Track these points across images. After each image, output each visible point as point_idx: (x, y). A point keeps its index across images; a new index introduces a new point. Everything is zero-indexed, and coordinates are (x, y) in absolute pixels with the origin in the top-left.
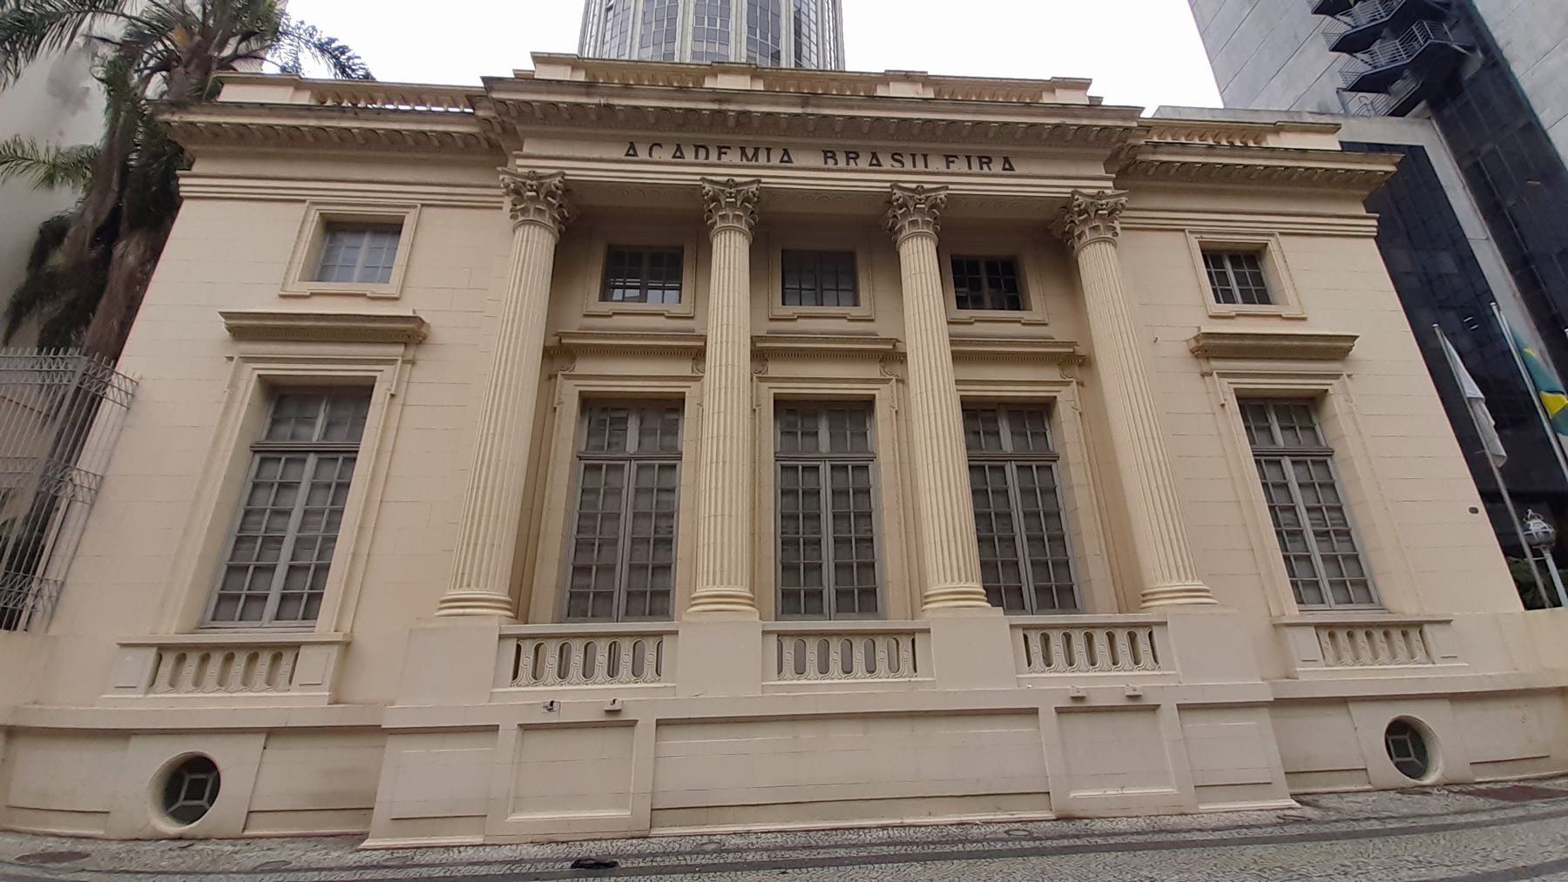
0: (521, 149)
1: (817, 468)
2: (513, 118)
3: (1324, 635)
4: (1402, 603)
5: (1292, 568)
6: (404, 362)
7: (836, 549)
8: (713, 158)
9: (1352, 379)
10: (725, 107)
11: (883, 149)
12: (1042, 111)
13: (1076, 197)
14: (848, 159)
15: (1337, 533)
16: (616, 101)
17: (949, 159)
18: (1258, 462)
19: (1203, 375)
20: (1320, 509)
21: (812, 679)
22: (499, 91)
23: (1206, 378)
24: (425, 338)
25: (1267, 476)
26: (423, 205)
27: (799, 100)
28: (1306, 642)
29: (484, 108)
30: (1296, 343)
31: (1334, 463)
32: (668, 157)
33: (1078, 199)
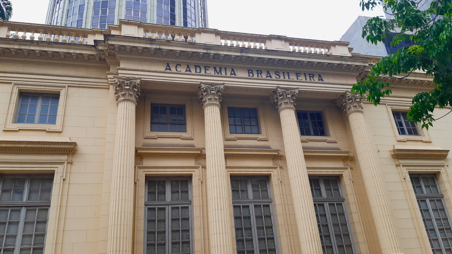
0: (119, 65)
1: (248, 206)
2: (117, 51)
5: (429, 234)
6: (68, 163)
7: (259, 243)
8: (203, 72)
9: (448, 167)
10: (209, 52)
11: (272, 70)
12: (333, 58)
13: (348, 93)
14: (258, 73)
15: (446, 229)
16: (163, 47)
17: (298, 75)
18: (418, 201)
19: (397, 166)
20: (440, 219)
22: (112, 40)
23: (398, 167)
24: (76, 151)
25: (421, 206)
26: (68, 86)
27: (239, 50)
29: (102, 46)
30: (429, 153)
31: (444, 200)
32: (183, 71)
33: (348, 94)
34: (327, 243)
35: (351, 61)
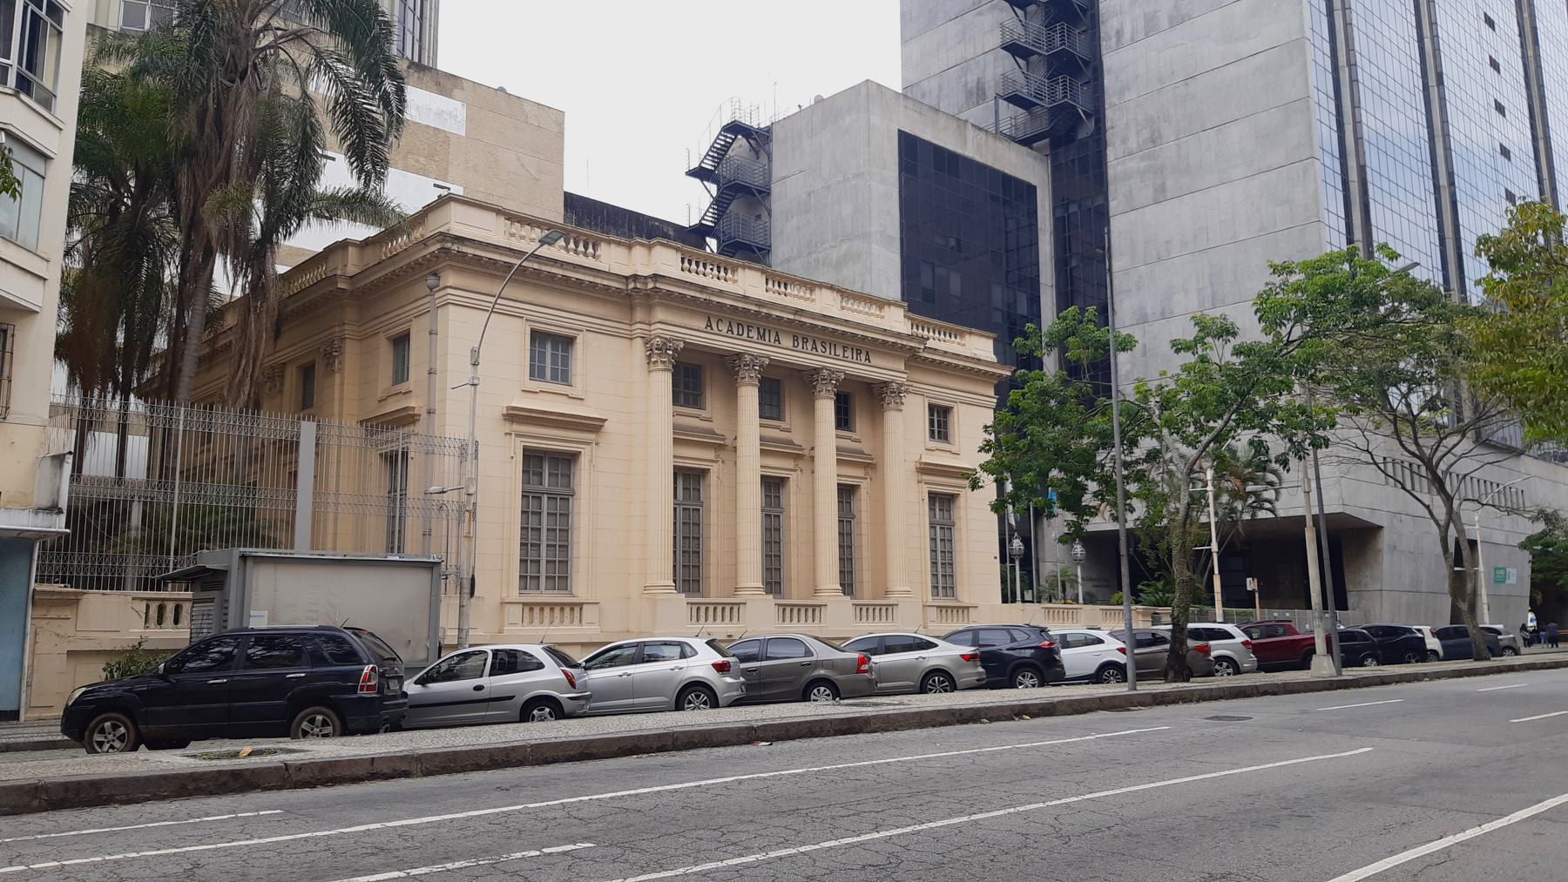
3: (527, 609)
4: (964, 598)
11: (819, 339)
19: (919, 482)
21: (787, 624)
28: (933, 613)
34: (532, 556)
35: (908, 340)
